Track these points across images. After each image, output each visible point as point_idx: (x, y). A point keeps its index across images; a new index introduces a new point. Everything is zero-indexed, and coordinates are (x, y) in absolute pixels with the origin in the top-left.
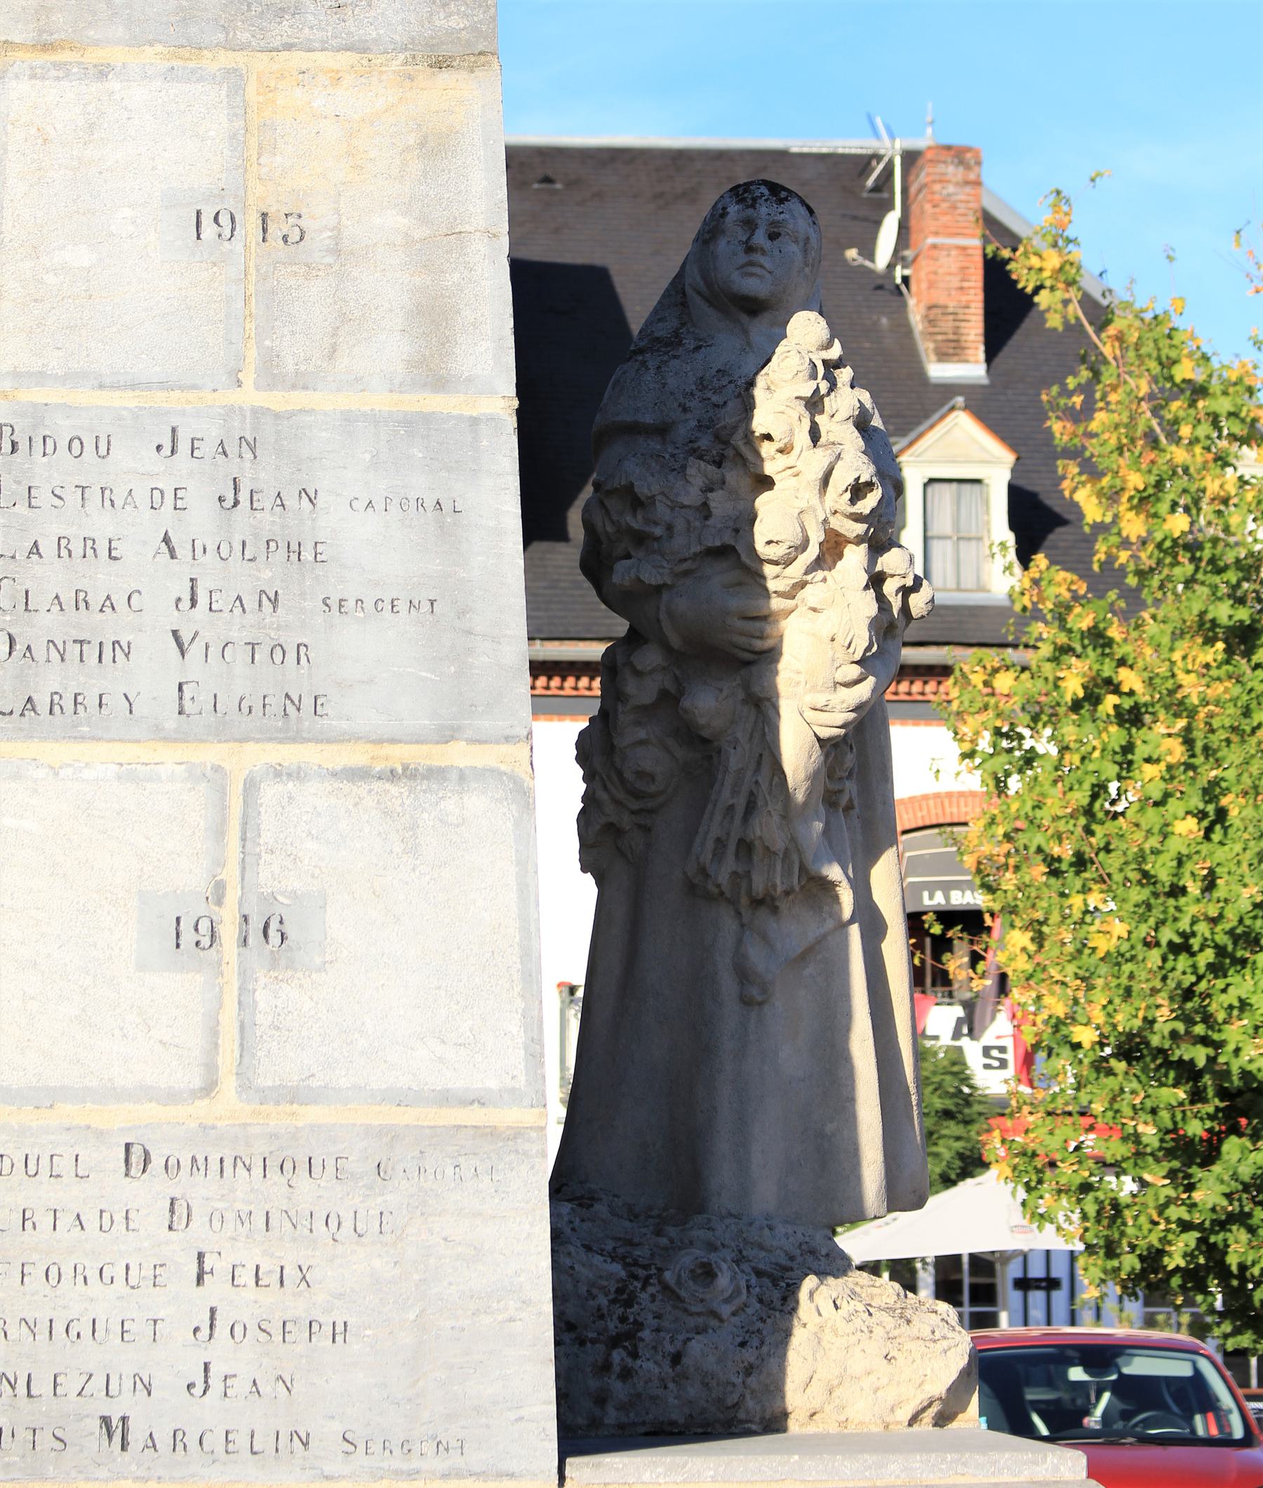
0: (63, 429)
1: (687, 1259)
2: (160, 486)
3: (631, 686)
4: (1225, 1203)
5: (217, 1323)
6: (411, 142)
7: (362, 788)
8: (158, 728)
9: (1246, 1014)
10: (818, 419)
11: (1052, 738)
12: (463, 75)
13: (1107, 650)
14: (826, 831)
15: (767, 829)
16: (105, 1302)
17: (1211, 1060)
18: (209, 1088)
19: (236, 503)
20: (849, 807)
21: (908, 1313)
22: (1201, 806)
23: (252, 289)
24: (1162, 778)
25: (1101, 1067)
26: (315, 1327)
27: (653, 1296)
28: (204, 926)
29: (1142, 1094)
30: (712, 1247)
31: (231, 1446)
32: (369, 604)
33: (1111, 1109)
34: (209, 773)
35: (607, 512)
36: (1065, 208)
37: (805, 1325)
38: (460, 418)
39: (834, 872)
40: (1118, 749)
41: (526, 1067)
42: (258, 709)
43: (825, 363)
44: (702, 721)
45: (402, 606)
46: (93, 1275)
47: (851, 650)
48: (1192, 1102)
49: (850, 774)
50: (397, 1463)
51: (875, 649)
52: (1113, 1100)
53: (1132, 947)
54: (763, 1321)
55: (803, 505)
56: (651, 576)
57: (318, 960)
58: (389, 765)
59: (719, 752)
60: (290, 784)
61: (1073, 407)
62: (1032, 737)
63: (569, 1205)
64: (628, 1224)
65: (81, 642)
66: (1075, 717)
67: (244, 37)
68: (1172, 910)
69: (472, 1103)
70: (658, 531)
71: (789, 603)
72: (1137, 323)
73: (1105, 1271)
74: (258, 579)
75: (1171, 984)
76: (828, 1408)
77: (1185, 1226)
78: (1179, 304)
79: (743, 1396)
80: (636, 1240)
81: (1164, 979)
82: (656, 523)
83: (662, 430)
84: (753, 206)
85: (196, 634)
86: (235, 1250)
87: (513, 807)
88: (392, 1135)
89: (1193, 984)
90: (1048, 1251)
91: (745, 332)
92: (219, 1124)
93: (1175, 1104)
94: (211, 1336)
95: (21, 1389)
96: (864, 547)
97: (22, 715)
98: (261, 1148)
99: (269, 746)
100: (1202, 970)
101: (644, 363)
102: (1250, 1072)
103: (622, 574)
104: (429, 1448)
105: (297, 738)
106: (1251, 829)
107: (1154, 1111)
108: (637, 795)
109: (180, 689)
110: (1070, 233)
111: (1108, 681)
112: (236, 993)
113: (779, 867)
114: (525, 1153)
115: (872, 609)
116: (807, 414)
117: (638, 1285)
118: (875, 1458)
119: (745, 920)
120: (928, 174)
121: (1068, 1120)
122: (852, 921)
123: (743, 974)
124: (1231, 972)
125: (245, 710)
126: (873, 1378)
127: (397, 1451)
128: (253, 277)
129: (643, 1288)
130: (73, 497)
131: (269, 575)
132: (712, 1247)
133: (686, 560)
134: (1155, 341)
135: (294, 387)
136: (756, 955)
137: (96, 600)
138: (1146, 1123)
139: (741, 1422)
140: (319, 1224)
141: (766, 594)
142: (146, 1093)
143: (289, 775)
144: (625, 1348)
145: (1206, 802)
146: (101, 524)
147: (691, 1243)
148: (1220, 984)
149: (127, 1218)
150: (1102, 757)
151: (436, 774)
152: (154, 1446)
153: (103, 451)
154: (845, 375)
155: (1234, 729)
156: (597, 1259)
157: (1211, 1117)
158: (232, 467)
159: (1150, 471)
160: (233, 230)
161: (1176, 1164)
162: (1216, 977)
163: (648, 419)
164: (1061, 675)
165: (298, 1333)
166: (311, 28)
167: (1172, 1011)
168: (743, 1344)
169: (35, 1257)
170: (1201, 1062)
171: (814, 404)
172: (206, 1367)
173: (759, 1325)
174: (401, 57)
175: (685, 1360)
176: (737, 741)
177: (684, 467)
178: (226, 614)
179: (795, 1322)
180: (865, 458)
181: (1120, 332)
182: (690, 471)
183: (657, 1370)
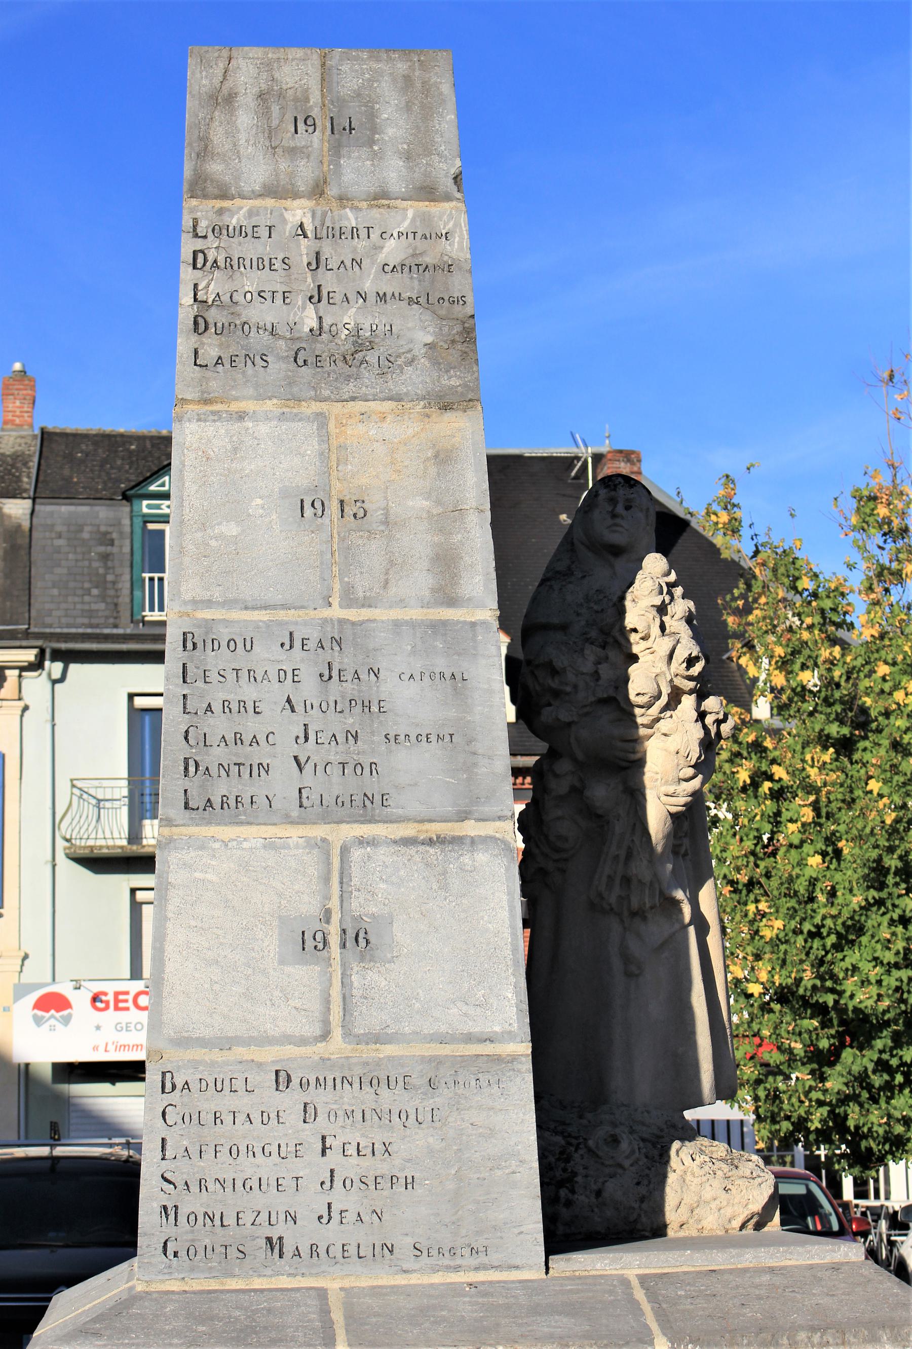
0: (224, 634)
1: (602, 1132)
2: (284, 668)
3: (553, 784)
4: (845, 1088)
5: (335, 1179)
6: (430, 455)
7: (412, 850)
8: (287, 816)
9: (856, 973)
10: (664, 618)
11: (728, 810)
12: (459, 413)
13: (764, 755)
14: (673, 869)
15: (640, 869)
16: (266, 1167)
17: (836, 1002)
18: (325, 1036)
19: (330, 677)
20: (685, 855)
21: (736, 1162)
22: (824, 848)
23: (335, 547)
24: (799, 831)
25: (765, 1008)
28: (319, 936)
29: (793, 1024)
30: (614, 1125)
31: (346, 1254)
32: (413, 738)
33: (775, 1033)
34: (319, 843)
35: (536, 677)
36: (732, 486)
37: (675, 1171)
38: (465, 622)
39: (679, 894)
40: (771, 814)
41: (518, 1018)
43: (668, 584)
45: (433, 738)
46: (258, 1151)
47: (689, 759)
48: (822, 1029)
49: (686, 834)
50: (446, 1261)
51: (703, 757)
52: (776, 1028)
53: (786, 935)
54: (650, 1169)
55: (658, 671)
56: (564, 716)
57: (389, 956)
58: (429, 835)
59: (608, 823)
60: (369, 849)
61: (738, 607)
62: (715, 808)
65: (239, 764)
66: (743, 796)
67: (326, 393)
68: (809, 911)
69: (485, 1041)
70: (568, 689)
71: (650, 731)
72: (774, 556)
73: (771, 1132)
74: (345, 724)
75: (812, 957)
76: (691, 1221)
77: (820, 1103)
78: (798, 543)
79: (639, 1215)
81: (808, 954)
82: (567, 684)
83: (564, 628)
84: (615, 490)
85: (309, 758)
86: (345, 1134)
87: (505, 860)
88: (437, 1061)
89: (823, 957)
90: (728, 1121)
91: (612, 566)
92: (332, 1057)
93: (811, 1029)
95: (217, 1222)
96: (694, 695)
97: (205, 810)
98: (358, 1071)
99: (355, 826)
100: (828, 948)
101: (551, 587)
102: (860, 1009)
103: (547, 715)
105: (372, 821)
106: (859, 861)
107: (800, 1034)
109: (300, 792)
110: (735, 500)
111: (765, 773)
112: (340, 977)
113: (647, 892)
114: (519, 1071)
115: (701, 734)
116: (658, 616)
117: (573, 1149)
118: (736, 1251)
120: (609, 468)
121: (746, 1041)
122: (690, 924)
123: (627, 958)
124: (846, 948)
125: (340, 804)
126: (717, 1202)
127: (447, 1254)
128: (336, 540)
129: (576, 1151)
130: (231, 676)
131: (351, 721)
132: (614, 1125)
133: (586, 706)
134: (786, 565)
135: (363, 606)
136: (634, 946)
137: (247, 738)
138: (796, 1041)
139: (639, 1231)
141: (636, 726)
142: (287, 1039)
143: (368, 843)
144: (567, 1188)
145: (827, 846)
146: (249, 692)
147: (601, 1122)
148: (840, 956)
149: (278, 1116)
150: (762, 819)
151: (457, 840)
152: (299, 1255)
153: (248, 647)
154: (678, 591)
155: (843, 801)
157: (833, 1037)
158: (327, 655)
159: (788, 646)
160: (323, 511)
161: (815, 1066)
162: (837, 952)
163: (555, 620)
164: (735, 770)
165: (385, 1184)
166: (367, 387)
167: (813, 973)
168: (638, 1184)
170: (831, 1004)
171: (662, 610)
172: (329, 1205)
173: (647, 1171)
174: (422, 403)
177: (582, 650)
178: (326, 746)
179: (669, 1169)
180: (693, 642)
181: (764, 561)
182: (587, 652)
183: (587, 1201)
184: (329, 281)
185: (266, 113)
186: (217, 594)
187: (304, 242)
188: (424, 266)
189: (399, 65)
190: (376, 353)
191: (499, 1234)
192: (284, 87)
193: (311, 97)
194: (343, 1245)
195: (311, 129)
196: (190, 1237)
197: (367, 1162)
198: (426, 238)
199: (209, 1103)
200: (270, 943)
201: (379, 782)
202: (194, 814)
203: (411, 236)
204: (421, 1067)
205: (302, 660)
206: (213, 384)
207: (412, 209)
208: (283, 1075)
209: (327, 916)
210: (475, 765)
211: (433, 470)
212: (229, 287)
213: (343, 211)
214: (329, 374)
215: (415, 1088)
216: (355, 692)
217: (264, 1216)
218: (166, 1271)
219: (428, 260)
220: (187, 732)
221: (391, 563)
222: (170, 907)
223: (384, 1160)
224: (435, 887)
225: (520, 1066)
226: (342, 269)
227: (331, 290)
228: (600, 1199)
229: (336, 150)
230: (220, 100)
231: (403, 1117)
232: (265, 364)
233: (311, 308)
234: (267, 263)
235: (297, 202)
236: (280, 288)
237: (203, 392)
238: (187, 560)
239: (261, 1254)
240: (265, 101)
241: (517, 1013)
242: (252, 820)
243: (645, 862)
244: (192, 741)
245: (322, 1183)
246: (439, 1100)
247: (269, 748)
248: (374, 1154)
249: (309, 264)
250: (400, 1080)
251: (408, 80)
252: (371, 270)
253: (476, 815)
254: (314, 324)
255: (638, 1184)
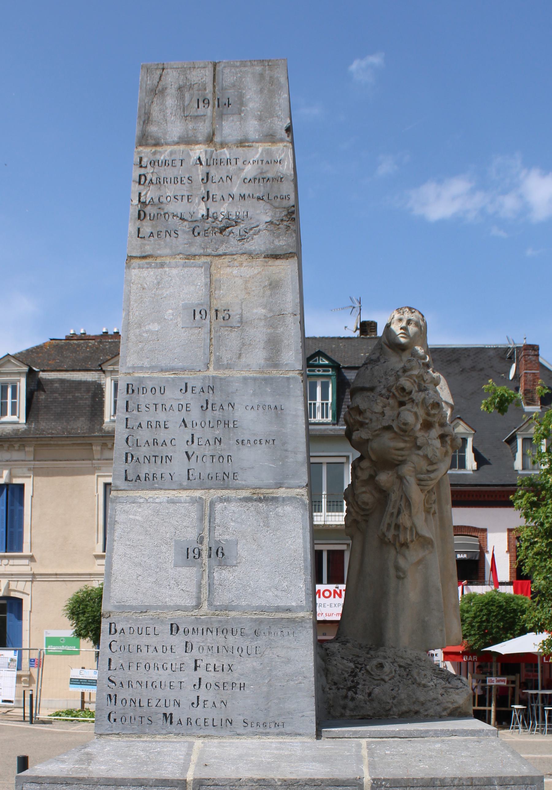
1: (375, 662)
2: (182, 403)
6: (266, 284)
7: (250, 504)
16: (164, 676)
18: (198, 606)
19: (207, 408)
20: (434, 513)
26: (234, 685)
27: (363, 674)
28: (196, 551)
32: (252, 442)
35: (351, 416)
42: (214, 478)
44: (382, 484)
45: (263, 442)
46: (160, 667)
50: (261, 730)
54: (400, 682)
57: (235, 562)
63: (339, 644)
64: (358, 650)
65: (155, 456)
69: (287, 610)
70: (367, 421)
74: (214, 434)
80: (360, 655)
82: (367, 419)
83: (372, 389)
84: (403, 314)
85: (194, 453)
87: (301, 510)
88: (260, 622)
94: (199, 687)
95: (137, 704)
97: (136, 481)
98: (216, 625)
101: (367, 368)
103: (356, 436)
104: (273, 725)
108: (363, 510)
114: (305, 627)
117: (358, 670)
119: (398, 550)
123: (397, 568)
125: (210, 478)
127: (261, 726)
129: (360, 671)
130: (153, 408)
133: (376, 431)
135: (226, 368)
136: (402, 562)
140: (235, 651)
142: (178, 608)
144: (353, 691)
146: (162, 416)
149: (171, 649)
153: (162, 392)
156: (345, 662)
158: (205, 396)
163: (367, 385)
168: (392, 690)
169: (141, 661)
173: (398, 683)
175: (372, 695)
176: (394, 491)
178: (204, 446)
182: (378, 401)
184: (214, 189)
185: (182, 98)
186: (146, 364)
187: (200, 168)
188: (267, 179)
189: (257, 68)
190: (238, 228)
191: (291, 716)
192: (193, 83)
193: (207, 88)
194: (205, 719)
195: (206, 106)
196: (122, 711)
197: (219, 675)
198: (268, 163)
199: (134, 640)
200: (169, 555)
201: (232, 466)
202: (130, 484)
203: (260, 162)
204: (251, 624)
205: (192, 399)
206: (148, 247)
207: (261, 148)
208: (174, 626)
209: (201, 540)
210: (287, 457)
211: (268, 292)
212: (158, 194)
213: (222, 150)
214: (211, 240)
215: (247, 635)
216: (221, 416)
217: (162, 702)
218: (109, 729)
219: (269, 175)
220: (127, 439)
221: (243, 344)
222: (116, 534)
223: (229, 674)
224: (261, 525)
225: (305, 625)
226: (221, 182)
227: (214, 194)
228: (370, 698)
229: (221, 116)
230: (157, 92)
231: (240, 650)
232: (176, 236)
233: (203, 204)
234: (179, 180)
235: (197, 147)
236: (186, 193)
237: (142, 252)
238: (130, 344)
239: (161, 722)
240: (181, 91)
241: (305, 596)
242: (161, 487)
243: (407, 516)
244: (130, 444)
245: (195, 685)
246: (260, 642)
247: (172, 447)
248: (223, 671)
249: (203, 179)
250: (239, 630)
251: (262, 76)
252: (237, 182)
253: (286, 485)
254: (205, 213)
255: (392, 690)
